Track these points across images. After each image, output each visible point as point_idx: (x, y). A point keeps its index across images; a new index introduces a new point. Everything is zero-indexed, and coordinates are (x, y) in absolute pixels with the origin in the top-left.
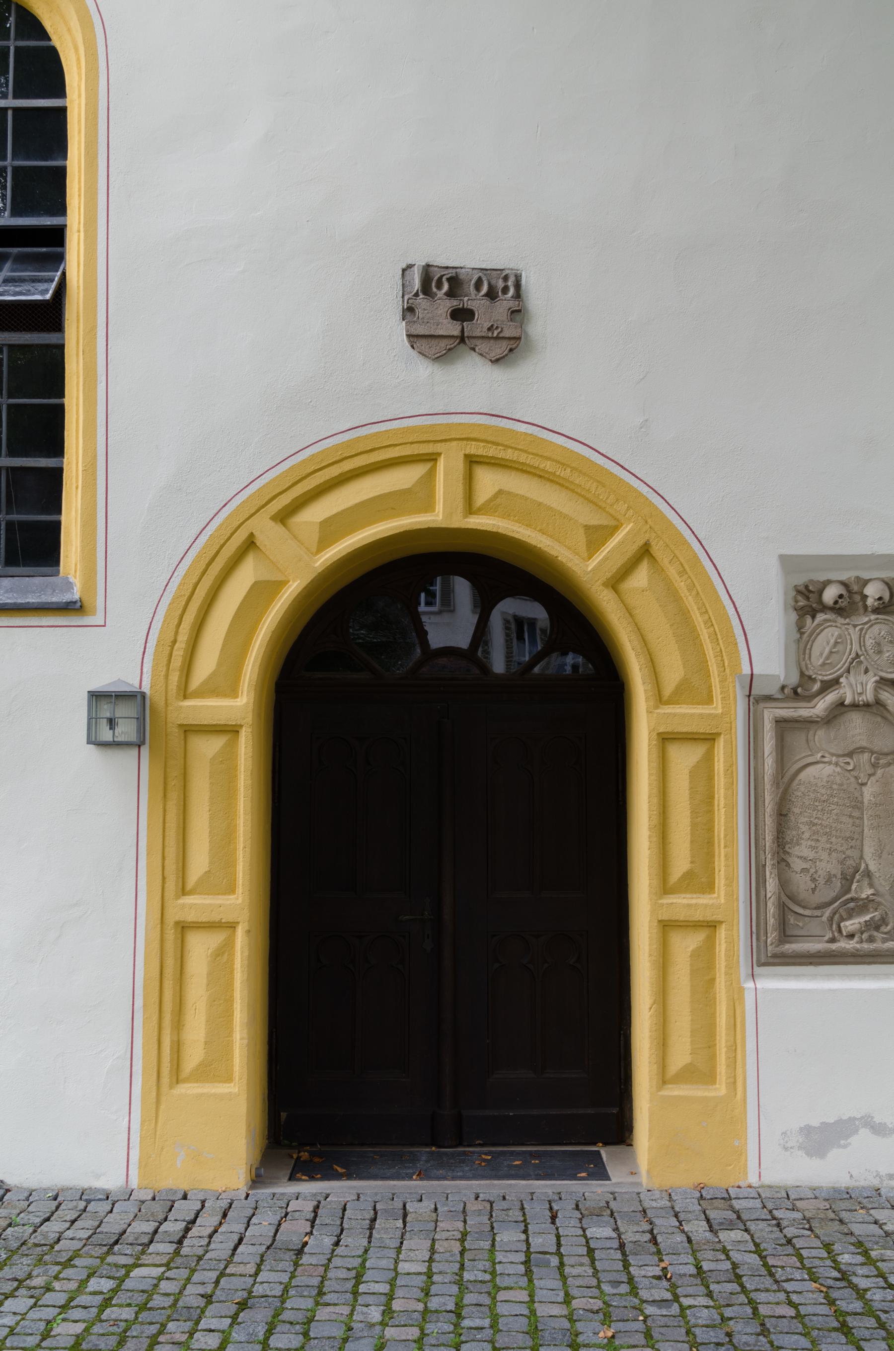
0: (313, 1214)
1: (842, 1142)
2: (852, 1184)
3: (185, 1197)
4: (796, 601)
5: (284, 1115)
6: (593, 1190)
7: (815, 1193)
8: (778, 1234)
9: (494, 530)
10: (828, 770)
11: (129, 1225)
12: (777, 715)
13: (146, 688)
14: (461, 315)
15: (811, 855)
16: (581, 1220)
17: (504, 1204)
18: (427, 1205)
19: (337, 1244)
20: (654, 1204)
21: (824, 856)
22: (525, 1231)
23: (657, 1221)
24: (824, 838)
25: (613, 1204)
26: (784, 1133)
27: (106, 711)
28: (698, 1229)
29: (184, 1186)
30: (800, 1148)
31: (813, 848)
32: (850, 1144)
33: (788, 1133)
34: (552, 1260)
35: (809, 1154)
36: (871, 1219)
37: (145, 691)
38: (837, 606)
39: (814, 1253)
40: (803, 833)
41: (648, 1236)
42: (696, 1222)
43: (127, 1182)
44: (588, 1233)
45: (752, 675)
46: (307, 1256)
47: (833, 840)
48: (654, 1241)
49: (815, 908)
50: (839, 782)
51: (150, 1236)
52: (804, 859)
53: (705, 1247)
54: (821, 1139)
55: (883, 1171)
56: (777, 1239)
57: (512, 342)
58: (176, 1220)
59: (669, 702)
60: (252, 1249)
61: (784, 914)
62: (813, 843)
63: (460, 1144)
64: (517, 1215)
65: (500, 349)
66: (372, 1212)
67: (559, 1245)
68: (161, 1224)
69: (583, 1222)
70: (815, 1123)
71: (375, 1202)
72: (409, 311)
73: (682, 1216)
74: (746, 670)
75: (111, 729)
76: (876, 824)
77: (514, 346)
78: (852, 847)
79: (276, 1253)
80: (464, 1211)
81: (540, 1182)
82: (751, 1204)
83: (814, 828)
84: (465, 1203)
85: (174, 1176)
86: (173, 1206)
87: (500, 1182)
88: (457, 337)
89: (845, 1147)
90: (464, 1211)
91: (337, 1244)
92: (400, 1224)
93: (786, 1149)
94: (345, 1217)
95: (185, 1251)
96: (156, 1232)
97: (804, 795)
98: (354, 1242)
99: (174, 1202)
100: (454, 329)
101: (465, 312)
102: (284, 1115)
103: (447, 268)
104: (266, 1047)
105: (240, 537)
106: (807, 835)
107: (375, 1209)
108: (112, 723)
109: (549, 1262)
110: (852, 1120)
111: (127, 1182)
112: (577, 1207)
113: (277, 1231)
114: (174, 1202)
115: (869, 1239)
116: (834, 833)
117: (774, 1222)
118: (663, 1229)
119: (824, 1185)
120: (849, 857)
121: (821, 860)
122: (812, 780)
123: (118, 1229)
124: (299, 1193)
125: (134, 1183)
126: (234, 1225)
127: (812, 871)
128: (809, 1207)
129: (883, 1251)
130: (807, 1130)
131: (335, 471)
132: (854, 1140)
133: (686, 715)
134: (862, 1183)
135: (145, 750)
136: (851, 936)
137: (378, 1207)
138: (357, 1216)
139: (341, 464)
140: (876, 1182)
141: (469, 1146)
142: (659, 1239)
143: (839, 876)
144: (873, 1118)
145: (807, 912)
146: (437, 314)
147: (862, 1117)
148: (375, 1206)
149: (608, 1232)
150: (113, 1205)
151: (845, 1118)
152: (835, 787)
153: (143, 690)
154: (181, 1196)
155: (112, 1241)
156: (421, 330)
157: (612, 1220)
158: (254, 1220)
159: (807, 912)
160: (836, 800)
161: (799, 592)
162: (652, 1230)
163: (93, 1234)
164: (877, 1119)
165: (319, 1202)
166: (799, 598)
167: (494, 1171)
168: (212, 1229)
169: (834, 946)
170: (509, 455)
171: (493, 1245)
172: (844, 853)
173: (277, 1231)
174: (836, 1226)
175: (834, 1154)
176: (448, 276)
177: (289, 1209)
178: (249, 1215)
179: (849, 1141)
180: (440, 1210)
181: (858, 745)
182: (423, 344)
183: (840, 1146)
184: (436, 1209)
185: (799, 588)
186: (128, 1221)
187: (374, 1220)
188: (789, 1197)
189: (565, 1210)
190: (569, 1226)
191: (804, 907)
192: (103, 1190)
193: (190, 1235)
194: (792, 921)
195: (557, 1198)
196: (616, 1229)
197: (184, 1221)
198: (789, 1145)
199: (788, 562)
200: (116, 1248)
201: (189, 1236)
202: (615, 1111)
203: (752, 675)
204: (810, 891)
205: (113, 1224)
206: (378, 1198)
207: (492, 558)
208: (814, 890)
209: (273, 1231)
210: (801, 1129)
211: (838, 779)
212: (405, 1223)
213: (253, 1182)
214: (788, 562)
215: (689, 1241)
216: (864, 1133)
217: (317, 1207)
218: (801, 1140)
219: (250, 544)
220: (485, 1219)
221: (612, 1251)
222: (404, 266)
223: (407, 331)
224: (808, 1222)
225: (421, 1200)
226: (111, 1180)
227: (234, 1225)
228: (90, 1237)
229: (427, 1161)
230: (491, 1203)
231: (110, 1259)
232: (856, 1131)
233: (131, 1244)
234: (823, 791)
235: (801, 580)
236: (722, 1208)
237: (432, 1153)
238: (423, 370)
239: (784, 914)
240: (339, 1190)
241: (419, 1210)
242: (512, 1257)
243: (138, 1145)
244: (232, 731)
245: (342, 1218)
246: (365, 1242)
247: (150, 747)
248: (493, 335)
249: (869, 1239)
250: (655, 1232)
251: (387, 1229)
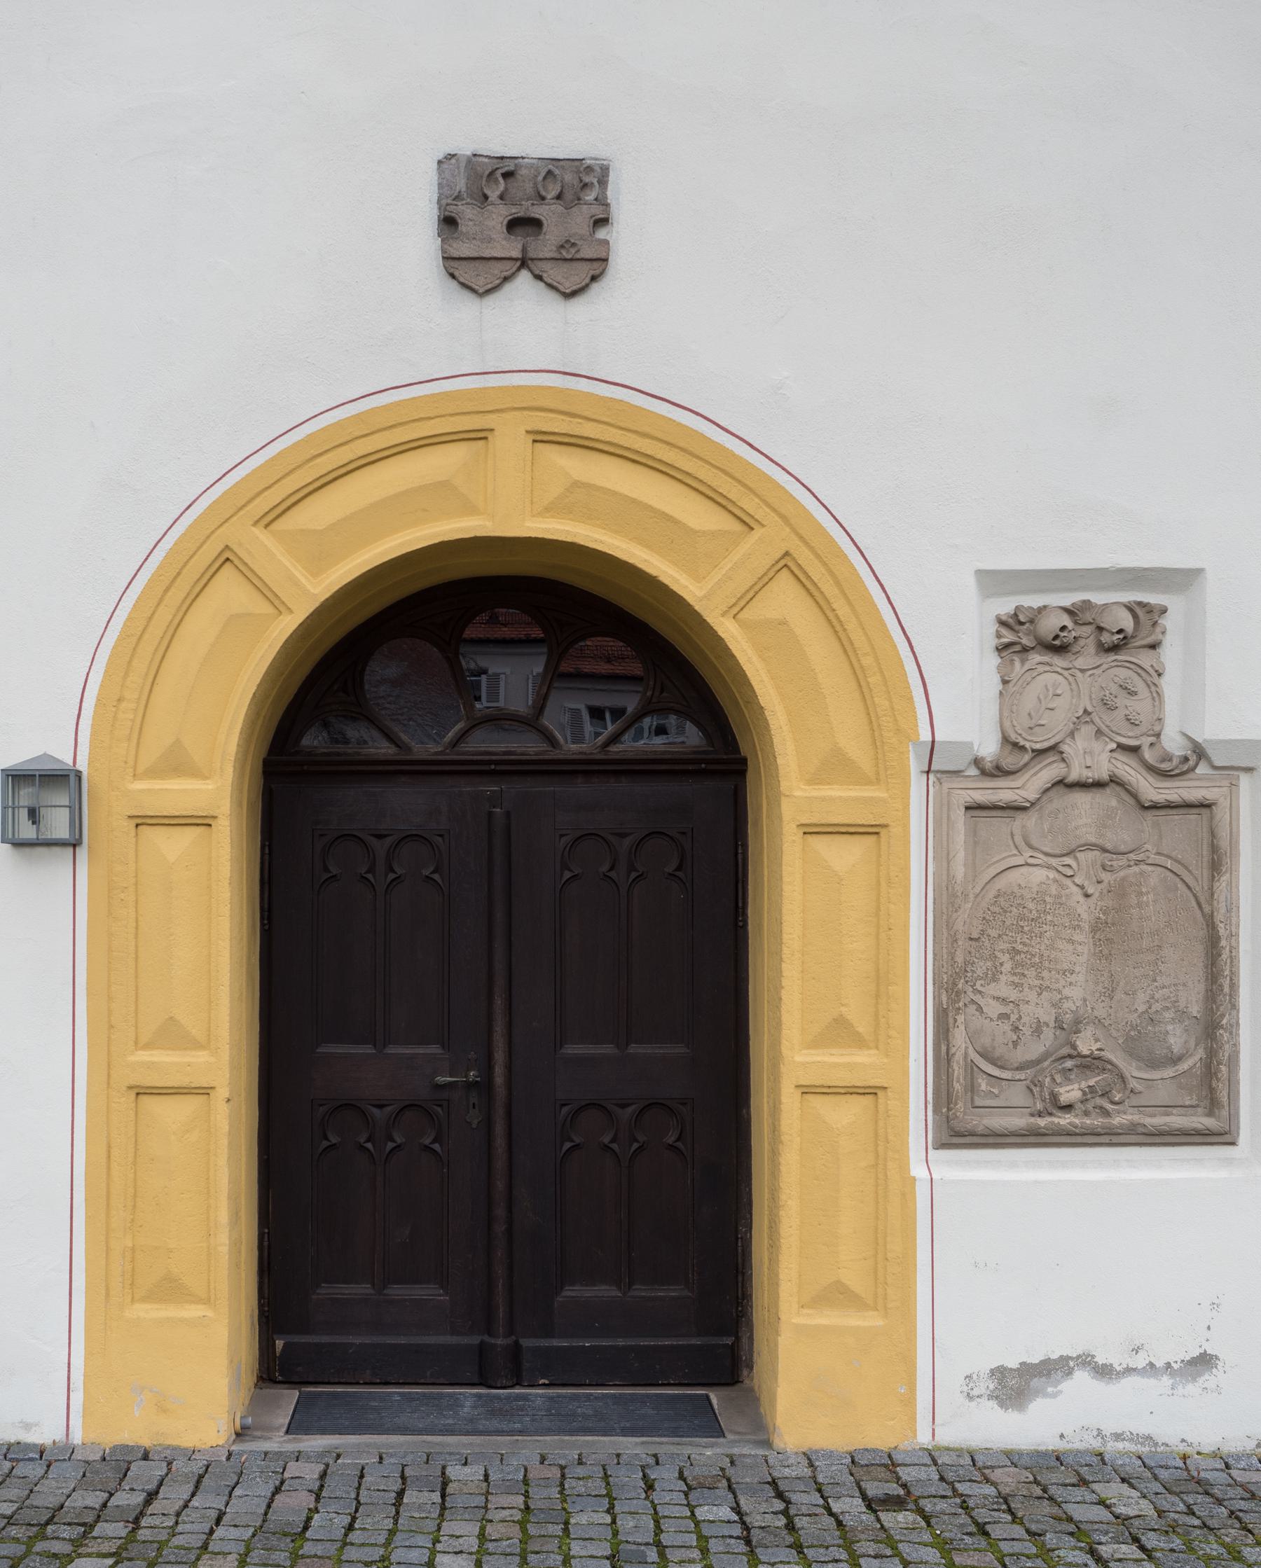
0: (318, 1484)
1: (1050, 1390)
2: (1061, 1446)
3: (146, 1457)
4: (999, 636)
5: (279, 1344)
6: (706, 1454)
7: (1012, 1458)
8: (964, 1519)
9: (569, 539)
10: (1039, 875)
11: (69, 1496)
12: (969, 799)
13: (82, 765)
14: (522, 225)
15: (1013, 995)
16: (686, 1495)
17: (580, 1471)
18: (473, 1473)
19: (350, 1528)
20: (787, 1472)
21: (1032, 996)
22: (610, 1510)
23: (794, 1497)
24: (1031, 973)
25: (730, 1472)
26: (969, 1377)
27: (26, 796)
28: (850, 1507)
29: (146, 1442)
30: (990, 1397)
31: (1016, 985)
32: (1061, 1392)
33: (975, 1377)
34: (648, 1553)
35: (1002, 1405)
36: (1094, 1498)
37: (80, 769)
38: (1057, 642)
39: (1017, 1547)
40: (1001, 964)
41: (782, 1521)
42: (848, 1500)
43: (67, 1435)
44: (698, 1512)
45: (933, 742)
46: (309, 1543)
47: (1045, 974)
48: (791, 1527)
49: (1017, 1069)
50: (1054, 892)
51: (96, 1513)
52: (1004, 1001)
53: (863, 1536)
54: (1016, 1385)
55: (1108, 1429)
56: (962, 1525)
57: (596, 265)
58: (132, 1489)
59: (147, 1046)
60: (234, 1533)
61: (972, 1079)
62: (1016, 979)
63: (518, 1384)
64: (598, 1487)
65: (581, 273)
66: (400, 1481)
67: (658, 1530)
68: (111, 1495)
69: (691, 1497)
70: (1013, 1363)
71: (404, 1466)
72: (448, 222)
73: (828, 1490)
74: (925, 736)
75: (34, 823)
76: (1106, 952)
77: (597, 272)
78: (1071, 984)
79: (267, 1539)
80: (526, 1481)
81: (630, 1439)
82: (922, 1474)
83: (1018, 958)
84: (526, 1470)
85: (134, 1428)
86: (128, 1469)
87: (574, 1438)
88: (516, 259)
89: (1054, 1396)
90: (526, 1481)
91: (350, 1528)
92: (436, 1497)
93: (970, 1397)
94: (363, 1487)
95: (143, 1534)
96: (105, 1505)
97: (1005, 912)
98: (375, 1522)
99: (130, 1463)
100: (512, 248)
101: (524, 220)
102: (279, 1344)
103: (502, 158)
104: (256, 1253)
105: (210, 551)
106: (1007, 967)
107: (403, 1477)
108: (33, 814)
109: (644, 1554)
110: (1064, 1359)
111: (67, 1435)
112: (681, 1477)
113: (269, 1506)
114: (130, 1463)
115: (1096, 1527)
116: (1046, 964)
117: (958, 1501)
118: (804, 1510)
119: (1023, 1447)
120: (1067, 998)
121: (1028, 1002)
122: (1016, 889)
123: (53, 1501)
124: (299, 1452)
125: (77, 1438)
126: (208, 1501)
127: (1013, 1017)
128: (1008, 1478)
129: (1116, 1546)
130: (1000, 1373)
131: (345, 454)
132: (1067, 1386)
133: (842, 799)
134: (1078, 1445)
135: (82, 853)
136: (1068, 1108)
137: (408, 1472)
138: (381, 1482)
139: (352, 445)
140: (1096, 1444)
141: (531, 1386)
142: (799, 1522)
143: (1052, 1024)
144: (1093, 1357)
145: (1006, 1075)
146: (488, 229)
147: (1079, 1357)
148: (403, 1471)
149: (725, 1512)
150: (48, 1466)
151: (1055, 1356)
152: (1048, 899)
153: (79, 767)
154: (140, 1455)
155: (44, 1519)
156: (464, 249)
157: (731, 1496)
158: (237, 1492)
159: (1006, 1075)
160: (1049, 918)
161: (1003, 623)
162: (787, 1508)
163: (18, 1509)
164: (1100, 1360)
165: (327, 1465)
166: (1004, 631)
167: (570, 1424)
168: (181, 1503)
169: (1042, 1122)
170: (589, 430)
171: (566, 1530)
172: (1060, 992)
173: (269, 1506)
174: (1046, 1507)
175: (1038, 1406)
176: (503, 171)
177: (286, 1475)
178: (232, 1484)
179: (1059, 1388)
180: (491, 1478)
181: (1083, 841)
182: (464, 271)
183: (1046, 1395)
184: (486, 1476)
185: (1004, 618)
186: (66, 1491)
187: (400, 1494)
188: (978, 1464)
189: (665, 1476)
190: (669, 1496)
191: (1002, 1067)
192: (35, 1445)
193: (150, 1510)
194: (983, 1087)
195: (651, 1461)
196: (737, 1509)
197: (143, 1490)
198: (975, 1392)
199: (993, 581)
200: (50, 1528)
201: (149, 1512)
202: (729, 1341)
203: (933, 742)
204: (1011, 1045)
205: (47, 1496)
206: (409, 1459)
207: (563, 584)
208: (1015, 1044)
209: (264, 1507)
210: (992, 1370)
211: (1054, 889)
212: (443, 1496)
213: (238, 1435)
214: (993, 581)
215: (840, 1524)
216: (1082, 1377)
217: (323, 1476)
218: (992, 1387)
219: (226, 558)
220: (554, 1492)
221: (733, 1541)
222: (441, 156)
223: (443, 251)
224: (1006, 1502)
225: (465, 1464)
226: (46, 1433)
227: (208, 1501)
228: (14, 1513)
229: (474, 1407)
230: (562, 1468)
231: (40, 1546)
232: (1070, 1373)
233: (69, 1524)
234: (1031, 905)
235: (1005, 607)
236: (887, 1485)
237: (479, 1396)
238: (468, 306)
239: (972, 1079)
240: (355, 1447)
241: (465, 1476)
242: (593, 1549)
243: (82, 1386)
244: (204, 822)
245: (358, 1488)
246: (389, 1523)
247: (89, 852)
248: (567, 254)
249: (1096, 1527)
250: (792, 1512)
251: (421, 1499)
